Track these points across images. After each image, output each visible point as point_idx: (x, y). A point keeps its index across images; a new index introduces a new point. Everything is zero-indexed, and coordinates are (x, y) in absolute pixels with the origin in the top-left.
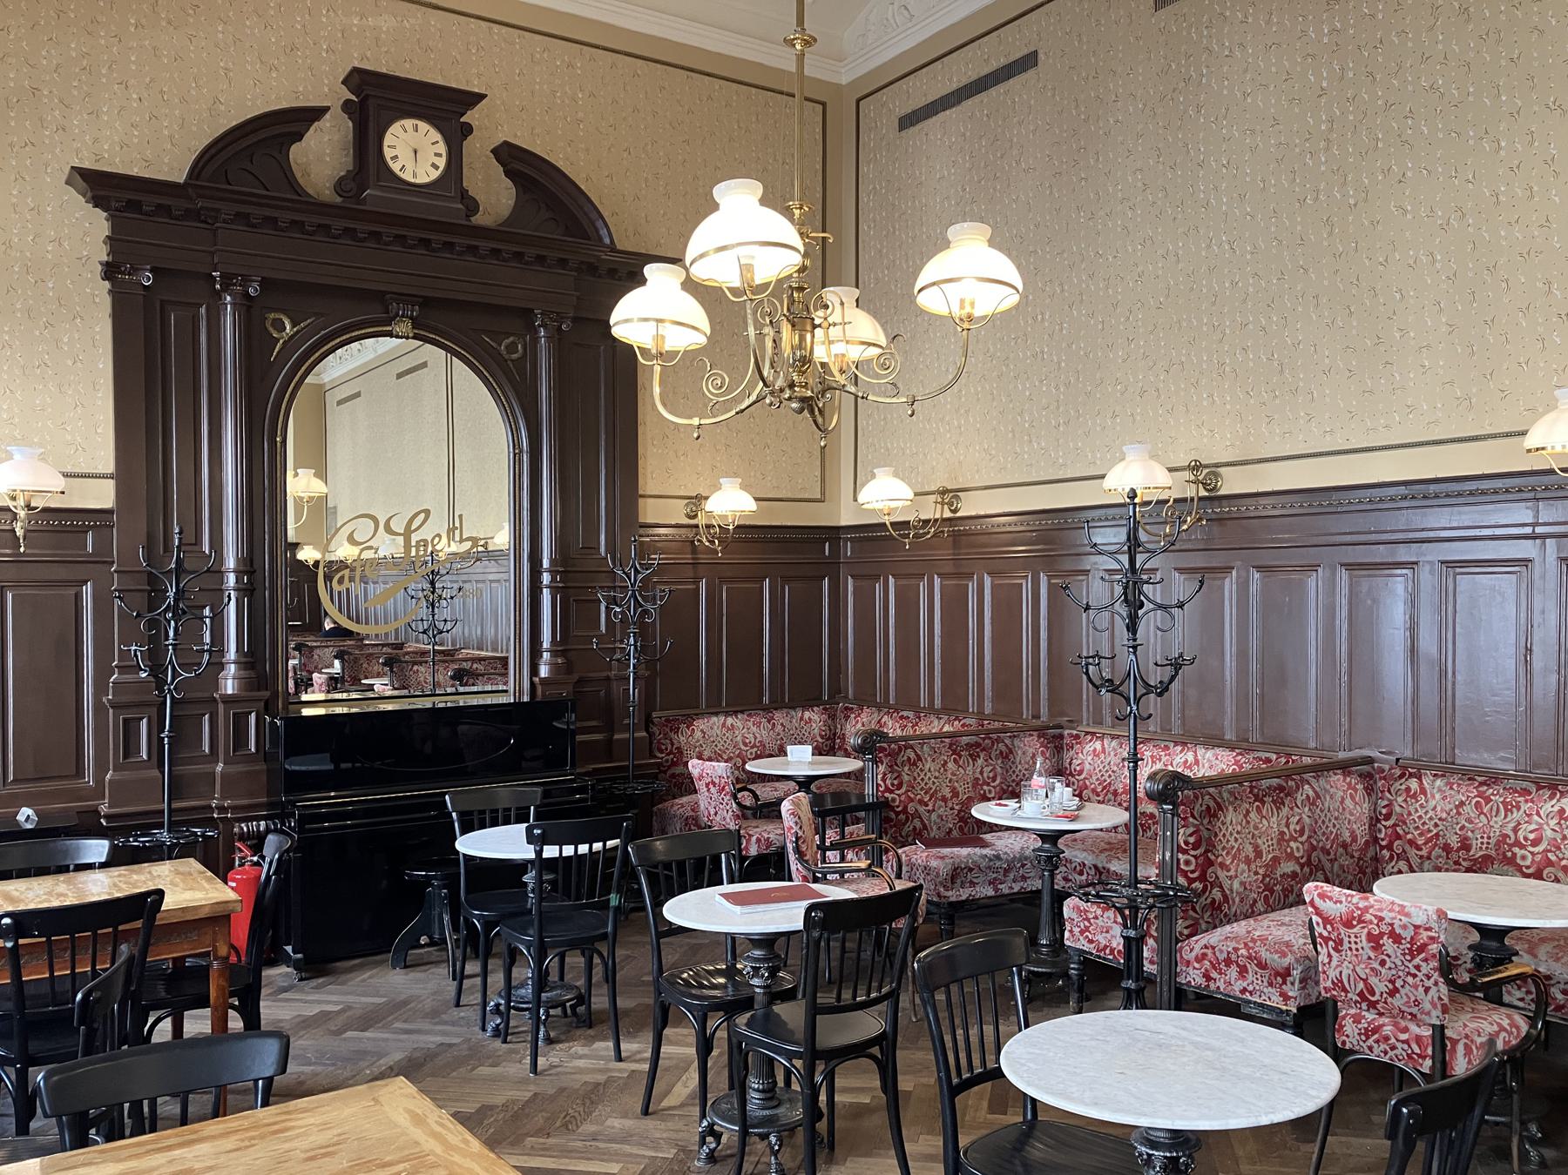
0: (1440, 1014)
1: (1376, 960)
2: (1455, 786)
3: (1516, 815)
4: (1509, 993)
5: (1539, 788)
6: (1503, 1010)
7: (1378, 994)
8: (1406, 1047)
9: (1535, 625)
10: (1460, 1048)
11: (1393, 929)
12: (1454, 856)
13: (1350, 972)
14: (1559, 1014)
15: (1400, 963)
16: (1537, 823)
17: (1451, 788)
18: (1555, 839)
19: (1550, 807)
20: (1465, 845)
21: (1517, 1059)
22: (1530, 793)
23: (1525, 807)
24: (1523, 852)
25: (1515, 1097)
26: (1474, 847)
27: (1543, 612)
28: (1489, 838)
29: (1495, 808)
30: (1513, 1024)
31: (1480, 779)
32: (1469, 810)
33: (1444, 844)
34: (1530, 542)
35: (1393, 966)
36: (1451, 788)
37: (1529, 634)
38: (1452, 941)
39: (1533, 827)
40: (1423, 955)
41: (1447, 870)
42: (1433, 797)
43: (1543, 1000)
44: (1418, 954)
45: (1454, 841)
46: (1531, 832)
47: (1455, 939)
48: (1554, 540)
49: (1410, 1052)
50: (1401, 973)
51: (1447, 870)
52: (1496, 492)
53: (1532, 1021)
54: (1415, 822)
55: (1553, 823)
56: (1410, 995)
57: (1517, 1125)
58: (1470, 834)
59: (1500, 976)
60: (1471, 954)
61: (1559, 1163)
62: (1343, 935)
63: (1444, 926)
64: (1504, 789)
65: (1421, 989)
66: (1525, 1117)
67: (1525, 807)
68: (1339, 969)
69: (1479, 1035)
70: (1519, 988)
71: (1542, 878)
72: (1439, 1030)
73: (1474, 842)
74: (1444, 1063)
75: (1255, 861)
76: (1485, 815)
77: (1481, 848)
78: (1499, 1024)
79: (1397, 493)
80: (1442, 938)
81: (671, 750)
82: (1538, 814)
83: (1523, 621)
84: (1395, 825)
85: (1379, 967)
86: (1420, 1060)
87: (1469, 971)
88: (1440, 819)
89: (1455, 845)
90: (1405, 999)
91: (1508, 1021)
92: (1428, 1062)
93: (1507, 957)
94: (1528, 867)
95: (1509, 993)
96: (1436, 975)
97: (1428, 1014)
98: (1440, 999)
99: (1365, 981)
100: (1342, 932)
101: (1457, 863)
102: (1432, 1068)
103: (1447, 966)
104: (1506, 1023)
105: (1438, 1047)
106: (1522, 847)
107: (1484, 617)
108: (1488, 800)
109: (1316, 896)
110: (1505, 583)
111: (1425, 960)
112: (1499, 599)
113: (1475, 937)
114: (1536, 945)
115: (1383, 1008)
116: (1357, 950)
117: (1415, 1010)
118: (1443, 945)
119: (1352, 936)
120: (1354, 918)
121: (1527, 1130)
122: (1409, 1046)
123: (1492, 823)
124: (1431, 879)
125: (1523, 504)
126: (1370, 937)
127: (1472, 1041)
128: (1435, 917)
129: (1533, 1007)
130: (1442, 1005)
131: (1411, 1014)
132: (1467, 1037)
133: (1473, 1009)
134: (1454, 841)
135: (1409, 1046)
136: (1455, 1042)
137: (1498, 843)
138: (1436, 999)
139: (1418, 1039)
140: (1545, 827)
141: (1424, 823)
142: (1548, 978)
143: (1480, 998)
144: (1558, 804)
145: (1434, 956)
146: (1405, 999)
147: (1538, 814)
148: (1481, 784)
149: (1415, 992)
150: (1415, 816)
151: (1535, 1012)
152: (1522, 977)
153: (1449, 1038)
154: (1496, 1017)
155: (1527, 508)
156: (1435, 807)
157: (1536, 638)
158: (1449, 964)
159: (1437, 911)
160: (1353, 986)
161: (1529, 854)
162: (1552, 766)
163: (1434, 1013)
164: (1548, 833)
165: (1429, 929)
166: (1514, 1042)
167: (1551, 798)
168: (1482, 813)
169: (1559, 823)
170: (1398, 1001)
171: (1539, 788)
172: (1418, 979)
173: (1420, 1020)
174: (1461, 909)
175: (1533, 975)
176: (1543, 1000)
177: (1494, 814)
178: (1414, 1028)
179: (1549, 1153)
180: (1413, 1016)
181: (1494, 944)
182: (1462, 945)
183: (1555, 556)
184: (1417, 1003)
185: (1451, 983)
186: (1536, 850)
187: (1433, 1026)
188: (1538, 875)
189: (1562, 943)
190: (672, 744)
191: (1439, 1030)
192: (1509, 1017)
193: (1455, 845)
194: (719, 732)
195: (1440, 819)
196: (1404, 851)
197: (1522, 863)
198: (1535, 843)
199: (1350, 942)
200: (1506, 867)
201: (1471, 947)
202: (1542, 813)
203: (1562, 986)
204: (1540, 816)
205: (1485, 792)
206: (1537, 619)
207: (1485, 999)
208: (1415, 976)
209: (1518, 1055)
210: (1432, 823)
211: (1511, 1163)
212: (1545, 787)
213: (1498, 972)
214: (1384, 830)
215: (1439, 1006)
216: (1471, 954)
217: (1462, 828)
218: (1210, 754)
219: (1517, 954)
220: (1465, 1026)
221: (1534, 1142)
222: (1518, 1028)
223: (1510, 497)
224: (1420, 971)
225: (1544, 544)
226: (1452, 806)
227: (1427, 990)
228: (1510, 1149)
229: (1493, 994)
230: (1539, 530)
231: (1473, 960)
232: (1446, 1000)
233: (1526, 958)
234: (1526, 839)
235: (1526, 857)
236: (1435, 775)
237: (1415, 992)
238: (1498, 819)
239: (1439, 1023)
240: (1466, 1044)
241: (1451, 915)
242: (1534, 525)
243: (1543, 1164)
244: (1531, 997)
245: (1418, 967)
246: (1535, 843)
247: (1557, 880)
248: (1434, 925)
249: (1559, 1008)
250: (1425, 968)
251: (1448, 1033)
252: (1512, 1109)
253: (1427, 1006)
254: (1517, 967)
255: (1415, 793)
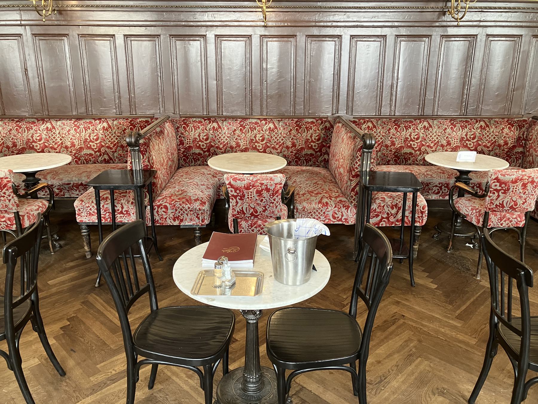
0: (16, 208)
1: (259, 200)
2: (7, 124)
3: (32, 131)
4: (39, 194)
5: (38, 121)
6: (39, 200)
7: (259, 212)
8: (5, 223)
9: (27, 60)
10: (26, 218)
11: (267, 187)
12: (11, 150)
13: (247, 206)
14: (57, 197)
15: (66, 140)
16: (206, 133)
17: (6, 125)
18: (47, 138)
19: (43, 127)
20: (15, 145)
21: (46, 215)
22: (35, 123)
23: (34, 128)
24: (36, 144)
25: (48, 228)
26: (18, 145)
27: (29, 55)
28: (23, 141)
29: (23, 130)
30: (43, 204)
31: (16, 120)
32: (14, 132)
33: (287, 146)
34: (20, 27)
35: (266, 201)
36: (6, 125)
37: (25, 64)
38: (16, 180)
39: (38, 135)
40: (6, 188)
41: (9, 155)
42: (280, 129)
43: (52, 193)
44: (4, 188)
45: (10, 144)
46: (38, 137)
47: (17, 179)
48: (29, 27)
49: (7, 224)
50: (268, 203)
51: (9, 155)
52: (4, 7)
53: (49, 201)
54: (52, 140)
55: (45, 132)
56: (3, 204)
57: (50, 237)
58: (394, 139)
59: (36, 189)
60: (24, 184)
61: (66, 245)
62: (245, 193)
63: (12, 176)
64: (26, 122)
65: (7, 201)
66: (52, 234)
67: (34, 128)
68: (242, 206)
69: (32, 211)
70: (43, 191)
71: (266, 153)
72: (17, 214)
73: (18, 143)
74: (21, 225)
75: (528, 182)
76: (300, 133)
77: (244, 145)
78: (38, 206)
79: (6, 4)
80: (12, 180)
81: (440, 187)
82: (39, 130)
83: (22, 58)
84: (322, 142)
85: (260, 203)
86: (11, 226)
87: (24, 190)
88: (3, 137)
89: (11, 146)
90: (269, 212)
91: (41, 204)
92: (15, 226)
93: (37, 182)
94: (39, 149)
95: (39, 194)
96: (12, 194)
97: (12, 209)
98: (15, 202)
99: (254, 208)
100: (245, 192)
101: (12, 152)
102: (17, 227)
103: (16, 190)
104: (40, 204)
105: (17, 220)
106: (36, 142)
107: (7, 57)
108: (20, 127)
109: (231, 180)
110: (13, 43)
111: (7, 190)
112: (12, 50)
113: (24, 177)
114: (46, 176)
115: (260, 217)
116: (251, 198)
117: (6, 209)
118: (13, 183)
119: (250, 193)
120: (251, 186)
121: (53, 237)
122: (6, 222)
123: (23, 135)
124: (4, 160)
125: (15, 12)
126: (257, 192)
127: (30, 214)
128: (8, 173)
129: (49, 196)
130: (16, 204)
131: (5, 211)
132: (27, 213)
133: (28, 203)
134: (10, 144)
135: (6, 222)
136: (23, 216)
137: (26, 143)
138: (14, 203)
139: (9, 219)
140: (42, 134)
141: (222, 139)
142: (52, 185)
143: (29, 198)
144: (46, 125)
145: (10, 187)
146: (269, 212)
147: (39, 130)
148: (17, 122)
149: (5, 203)
150: (486, 136)
151: (50, 198)
152: (43, 188)
153: (20, 215)
154: (37, 204)
155: (17, 14)
156: (380, 132)
157: (28, 65)
158: (16, 189)
159: (9, 171)
160: (248, 212)
161: (38, 145)
162: (42, 112)
163: (14, 208)
164: (44, 136)
165: (7, 178)
166: (44, 210)
167: (43, 124)
168: (243, 133)
169: (47, 132)
170: (267, 213)
171: (38, 121)
172: (5, 197)
173: (9, 212)
174: (17, 168)
175: (47, 186)
176: (52, 193)
177: (458, 130)
178: (7, 216)
179: (62, 243)
180: (6, 211)
181: (32, 178)
182: (20, 181)
183: (30, 33)
184: (6, 206)
185: (19, 196)
186: (40, 143)
187: (14, 213)
188: (43, 151)
189: (55, 173)
190: (436, 186)
191: (17, 214)
192: (41, 202)
193: (11, 146)
194: (185, 216)
195: (3, 137)
196: (215, 151)
197: (36, 148)
198: (40, 140)
199: (248, 195)
200: (31, 151)
201: (23, 181)
202: (40, 129)
203: (57, 187)
204: (97, 130)
205: (19, 124)
206: (27, 57)
207: (31, 198)
208: (4, 197)
209: (47, 214)
210: (59, 139)
211: (50, 250)
212: (40, 120)
213: (35, 188)
214: (96, 145)
215: (15, 205)
216: (24, 184)
217: (71, 139)
218: (59, 123)
219: (40, 180)
220: (26, 209)
221: (56, 241)
222: (45, 205)
223: (10, 9)
224: (5, 194)
225: (25, 28)
226: (7, 131)
227: (10, 200)
228: (49, 246)
229: (34, 196)
230: (23, 23)
231: (25, 185)
232: (17, 202)
233: (43, 180)
234: (36, 139)
235: (38, 147)
236: (113, 120)
237: (5, 203)
238: (192, 132)
239: (16, 211)
240: (28, 216)
241: (14, 171)
242: (21, 20)
243: (61, 247)
244: (47, 193)
245: (5, 193)
246: (40, 140)
247: (49, 152)
248: (9, 176)
249: (57, 195)
250: (7, 193)
251: (20, 214)
252: (47, 232)
253: (11, 206)
254: (41, 184)
255: (428, 128)
